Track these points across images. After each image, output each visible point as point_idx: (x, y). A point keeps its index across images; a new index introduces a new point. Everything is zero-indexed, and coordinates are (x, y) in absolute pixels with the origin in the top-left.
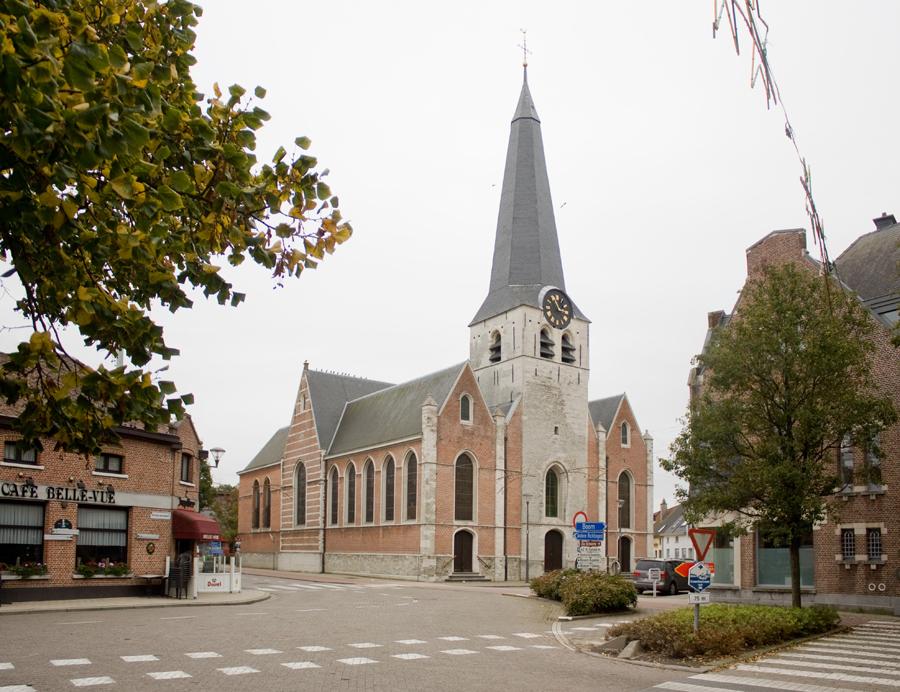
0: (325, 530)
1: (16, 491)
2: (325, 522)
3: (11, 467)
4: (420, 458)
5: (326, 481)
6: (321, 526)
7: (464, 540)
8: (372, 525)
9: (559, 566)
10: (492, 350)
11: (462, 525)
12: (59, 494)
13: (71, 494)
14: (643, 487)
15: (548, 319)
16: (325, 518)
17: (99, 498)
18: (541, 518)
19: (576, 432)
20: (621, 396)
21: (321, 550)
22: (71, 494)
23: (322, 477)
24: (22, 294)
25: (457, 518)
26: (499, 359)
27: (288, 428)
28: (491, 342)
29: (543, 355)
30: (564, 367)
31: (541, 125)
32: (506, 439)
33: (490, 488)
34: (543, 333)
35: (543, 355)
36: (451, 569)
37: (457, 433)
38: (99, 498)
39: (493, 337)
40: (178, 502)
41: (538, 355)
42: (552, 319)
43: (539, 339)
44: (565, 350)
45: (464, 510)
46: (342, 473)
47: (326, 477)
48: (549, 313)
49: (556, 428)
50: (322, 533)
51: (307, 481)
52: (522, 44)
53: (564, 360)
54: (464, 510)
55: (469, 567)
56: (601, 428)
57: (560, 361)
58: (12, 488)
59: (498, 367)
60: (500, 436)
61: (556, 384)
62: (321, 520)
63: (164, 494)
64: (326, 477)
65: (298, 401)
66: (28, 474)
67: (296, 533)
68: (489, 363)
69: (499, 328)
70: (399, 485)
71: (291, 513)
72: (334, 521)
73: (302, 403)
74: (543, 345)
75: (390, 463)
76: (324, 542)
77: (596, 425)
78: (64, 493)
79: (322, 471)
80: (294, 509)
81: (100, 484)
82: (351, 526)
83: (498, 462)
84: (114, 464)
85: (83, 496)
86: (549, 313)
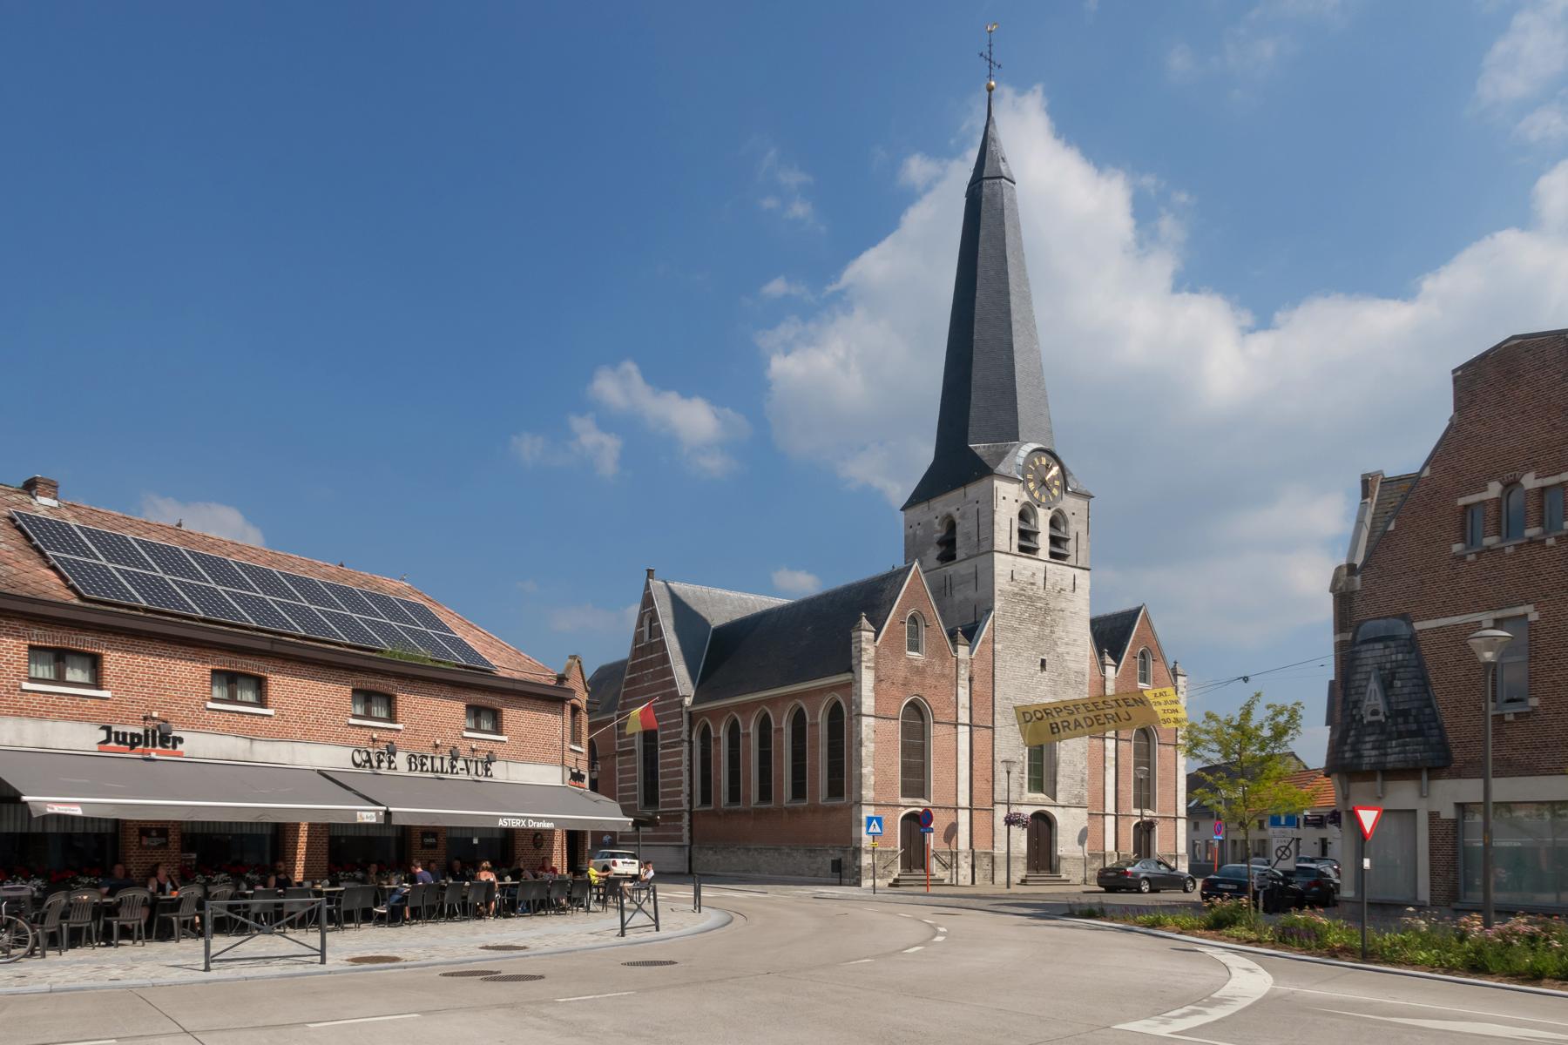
0: (691, 812)
1: (369, 761)
2: (691, 802)
3: (361, 727)
4: (849, 707)
5: (691, 742)
6: (686, 806)
7: (917, 824)
8: (741, 806)
9: (1148, 855)
10: (941, 543)
11: (917, 805)
12: (423, 765)
13: (437, 763)
14: (1171, 748)
15: (1031, 494)
16: (691, 795)
17: (473, 771)
18: (1022, 793)
19: (1071, 665)
20: (1139, 610)
21: (686, 841)
22: (437, 763)
23: (685, 736)
24: (1443, 816)
25: (903, 796)
26: (953, 557)
27: (624, 663)
28: (939, 531)
29: (1022, 549)
30: (1055, 568)
31: (1016, 187)
32: (971, 680)
33: (953, 749)
34: (1023, 516)
35: (1022, 549)
36: (897, 871)
37: (901, 672)
38: (473, 771)
39: (941, 524)
40: (568, 775)
41: (1015, 550)
42: (1036, 494)
43: (1016, 525)
44: (1055, 541)
45: (1145, 796)
46: (717, 731)
47: (690, 736)
48: (1031, 485)
49: (1043, 662)
50: (686, 816)
51: (660, 742)
52: (986, 52)
53: (1053, 555)
54: (1145, 796)
55: (923, 865)
56: (1108, 660)
57: (1047, 557)
58: (364, 756)
59: (951, 569)
60: (964, 673)
61: (1041, 592)
62: (684, 798)
63: (551, 763)
64: (690, 736)
65: (640, 624)
66: (386, 736)
67: (728, 813)
68: (937, 564)
69: (952, 509)
70: (815, 746)
71: (634, 788)
72: (706, 799)
73: (646, 628)
74: (1024, 534)
75: (799, 721)
76: (691, 830)
77: (1101, 654)
78: (429, 763)
79: (685, 727)
80: (639, 783)
81: (374, 740)
82: (837, 802)
83: (960, 711)
84: (379, 711)
85: (453, 767)
86: (1031, 485)
